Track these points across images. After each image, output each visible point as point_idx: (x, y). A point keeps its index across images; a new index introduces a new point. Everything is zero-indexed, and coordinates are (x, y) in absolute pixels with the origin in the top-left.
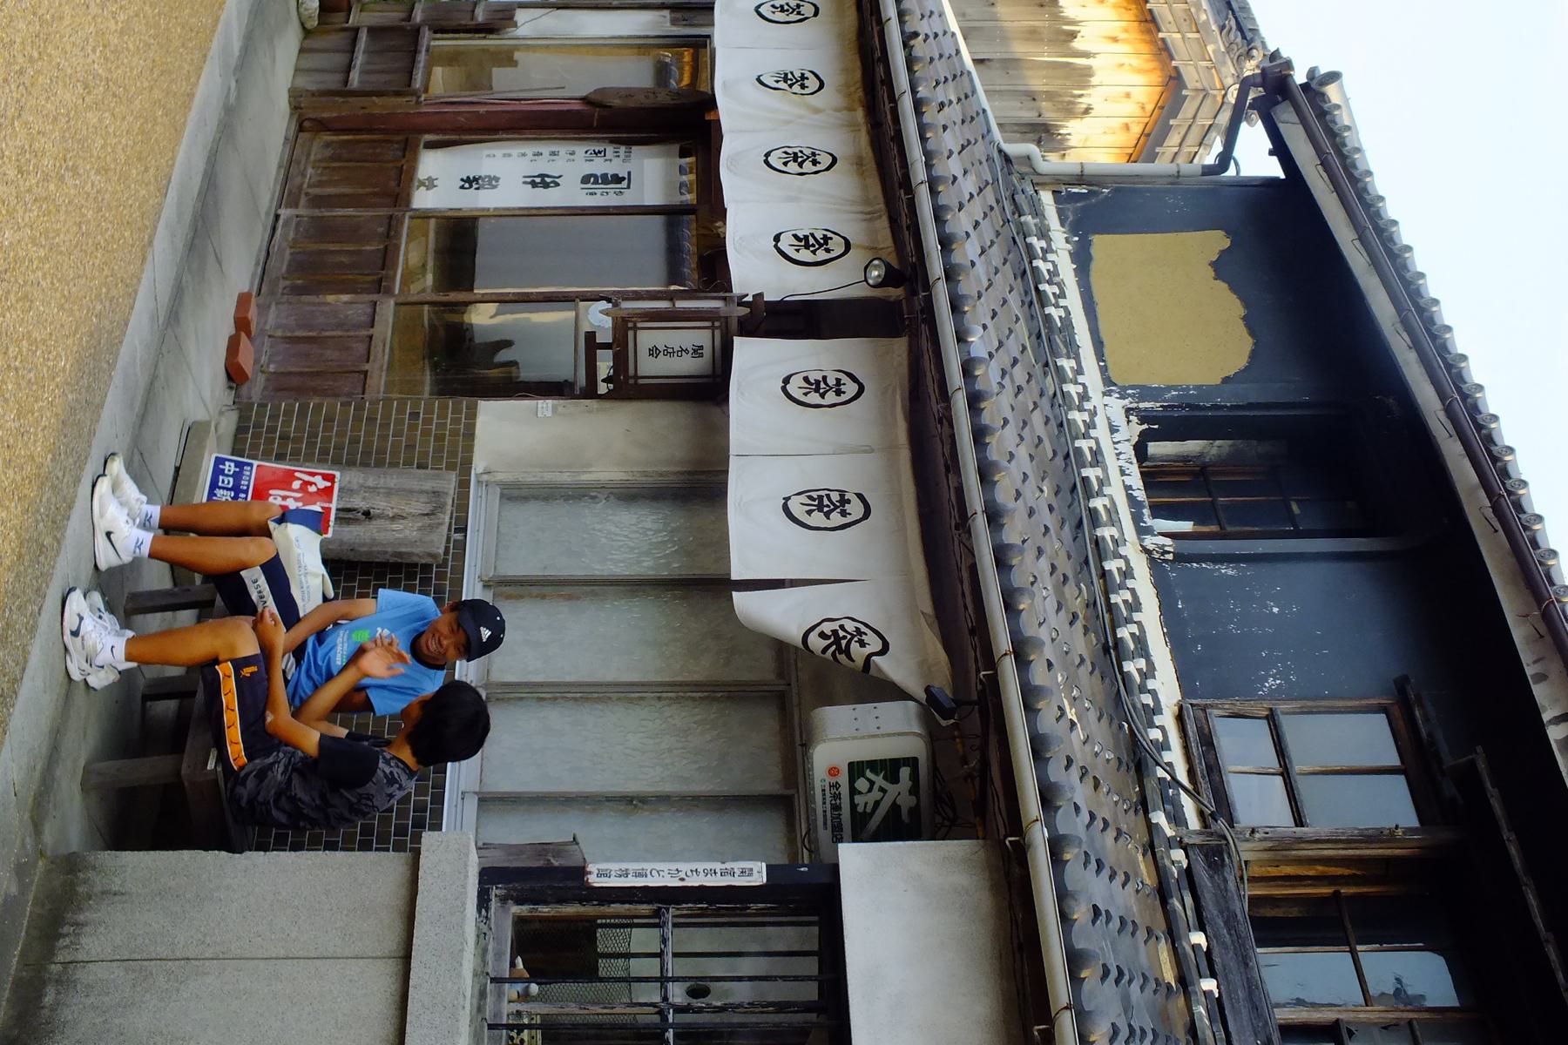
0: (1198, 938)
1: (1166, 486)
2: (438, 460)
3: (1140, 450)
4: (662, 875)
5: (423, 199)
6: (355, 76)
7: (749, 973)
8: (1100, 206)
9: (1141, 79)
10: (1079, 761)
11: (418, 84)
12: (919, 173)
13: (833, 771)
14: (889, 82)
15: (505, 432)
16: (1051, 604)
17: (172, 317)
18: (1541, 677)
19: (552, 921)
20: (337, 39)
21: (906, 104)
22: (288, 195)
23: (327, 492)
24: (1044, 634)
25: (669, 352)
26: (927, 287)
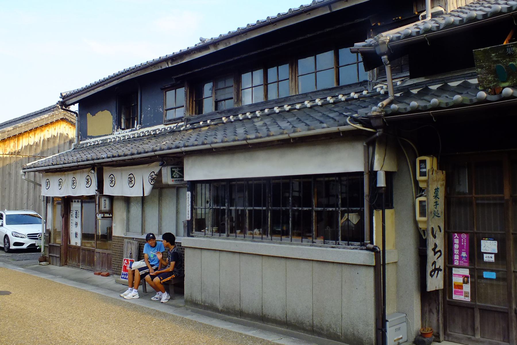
0: (201, 123)
1: (129, 125)
2: (122, 242)
3: (123, 129)
4: (189, 208)
5: (79, 244)
6: (57, 256)
7: (205, 194)
8: (82, 133)
9: (62, 125)
10: (172, 142)
11: (59, 245)
12: (76, 164)
13: (173, 181)
14: (60, 168)
15: (118, 231)
16: (147, 145)
17: (97, 286)
18: (161, 67)
19: (196, 225)
20: (51, 258)
21: (64, 165)
22: (78, 266)
23: (127, 260)
24: (152, 147)
25: (105, 205)
26: (95, 163)
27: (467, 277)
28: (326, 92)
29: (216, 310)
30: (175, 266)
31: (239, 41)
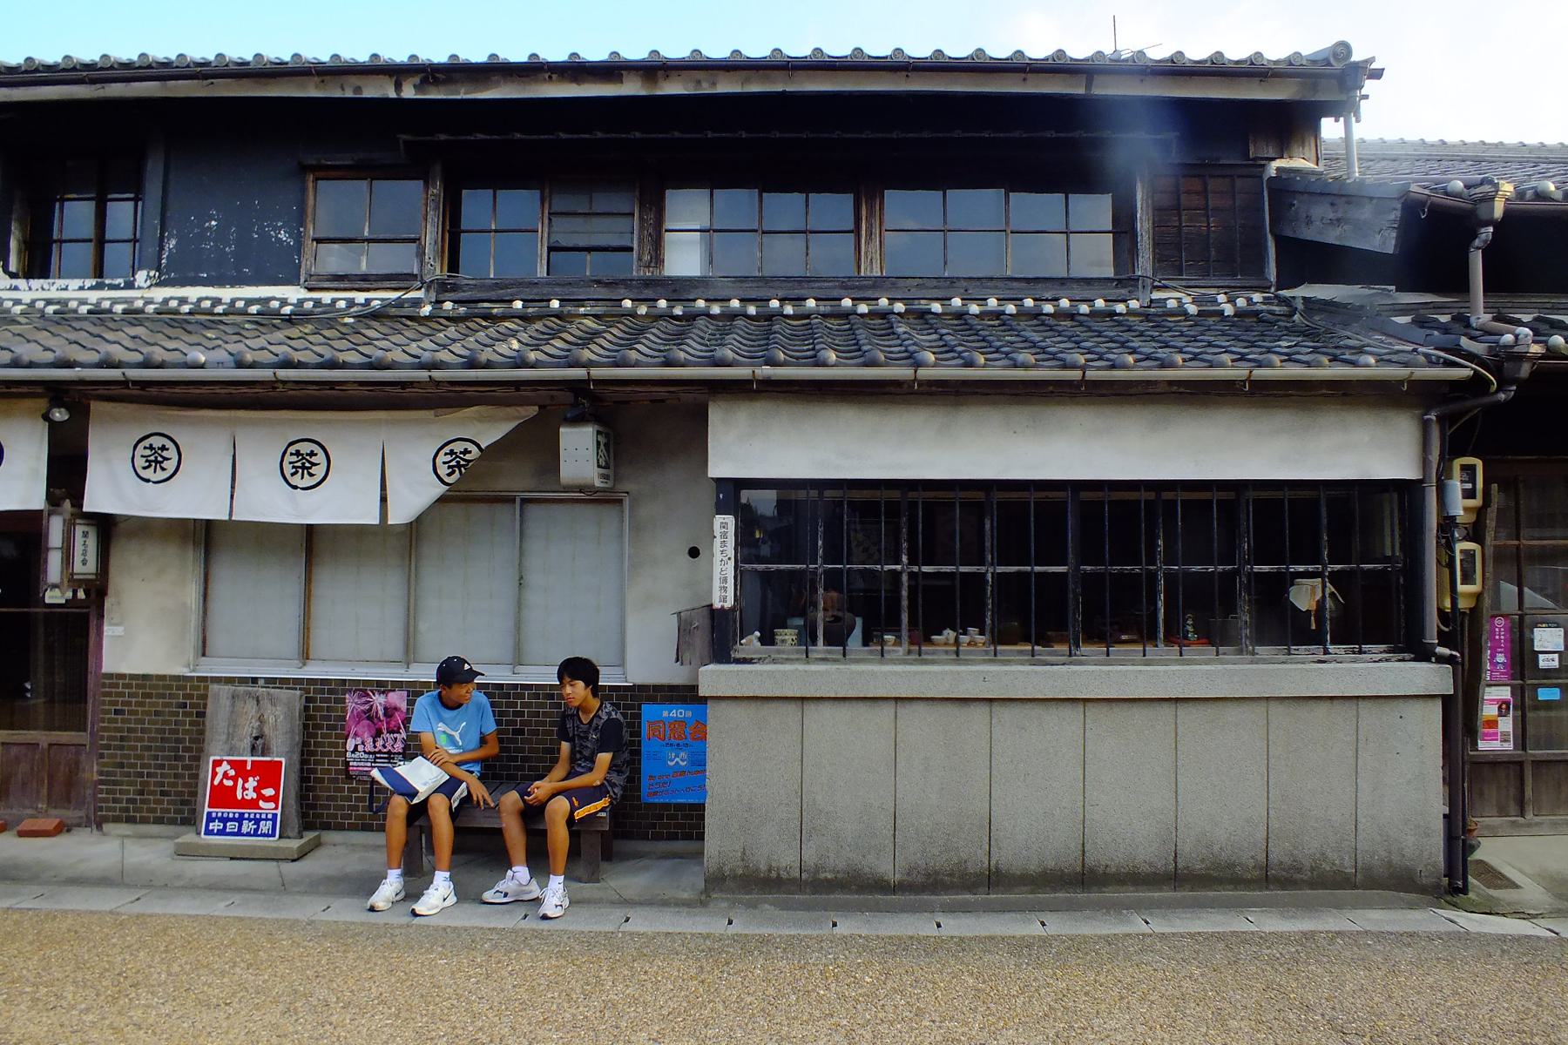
3: (13, 276)
18: (358, 89)
27: (1507, 703)
28: (1015, 284)
29: (880, 886)
30: (613, 767)
31: (755, 88)
